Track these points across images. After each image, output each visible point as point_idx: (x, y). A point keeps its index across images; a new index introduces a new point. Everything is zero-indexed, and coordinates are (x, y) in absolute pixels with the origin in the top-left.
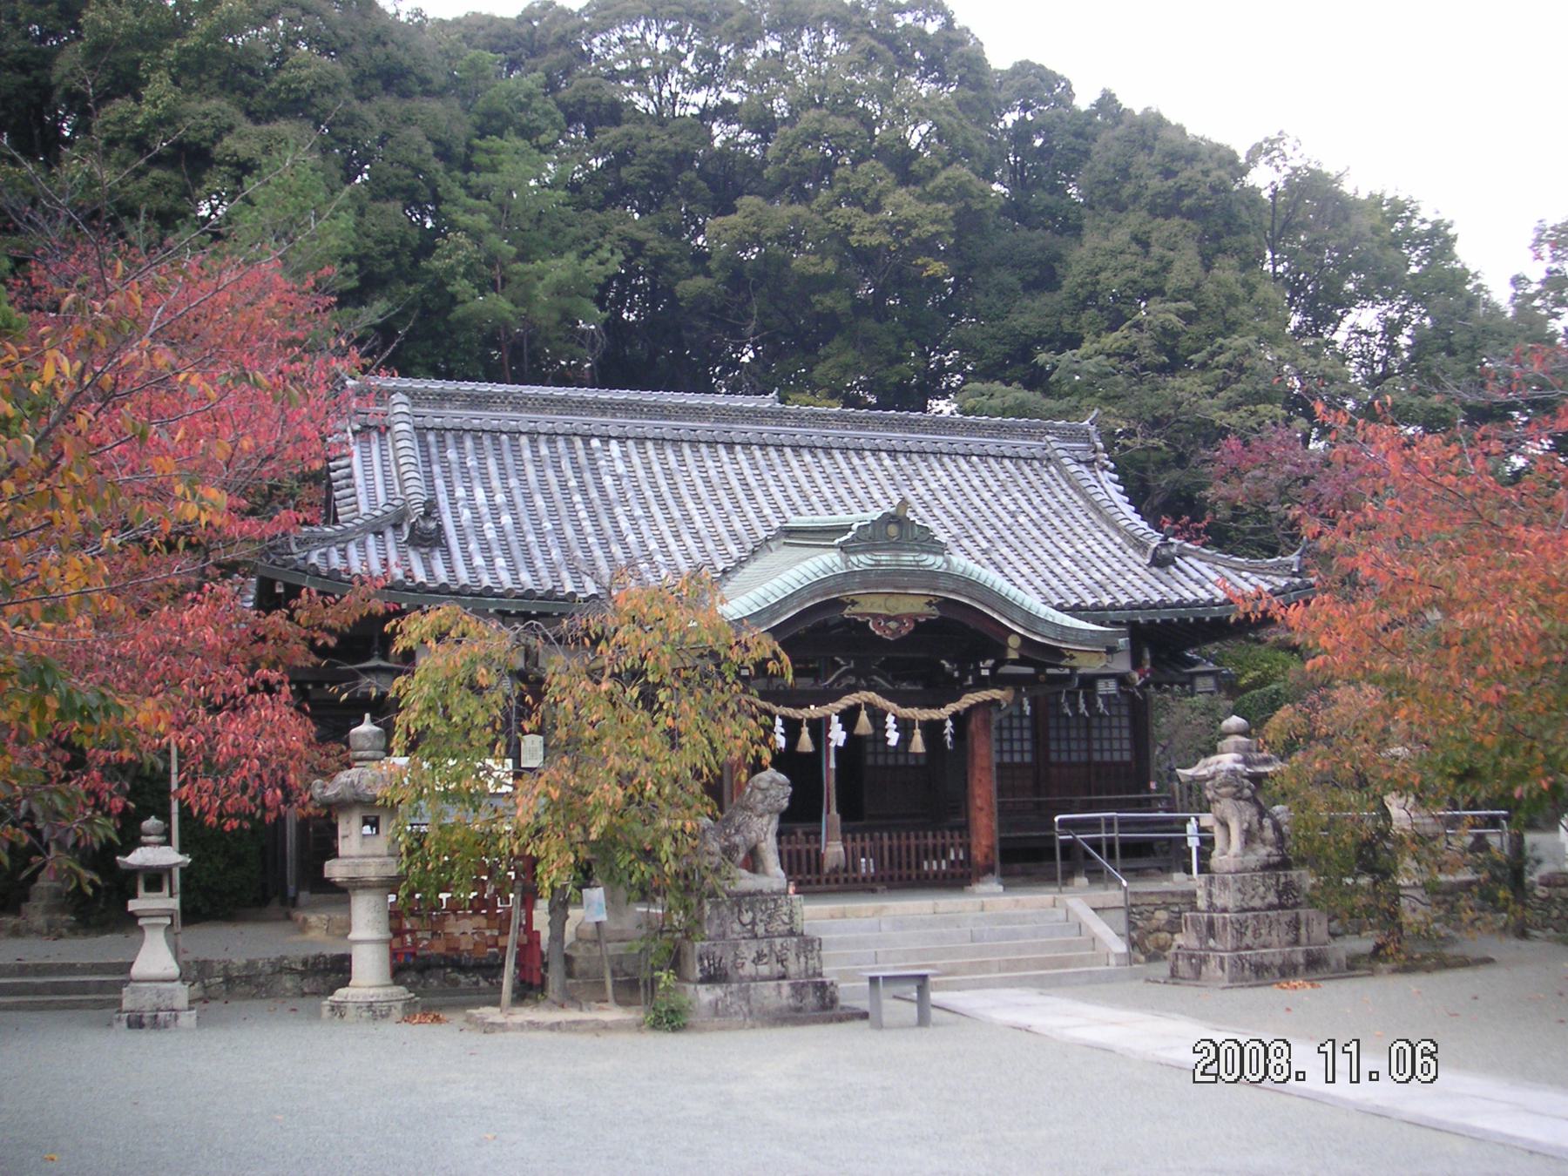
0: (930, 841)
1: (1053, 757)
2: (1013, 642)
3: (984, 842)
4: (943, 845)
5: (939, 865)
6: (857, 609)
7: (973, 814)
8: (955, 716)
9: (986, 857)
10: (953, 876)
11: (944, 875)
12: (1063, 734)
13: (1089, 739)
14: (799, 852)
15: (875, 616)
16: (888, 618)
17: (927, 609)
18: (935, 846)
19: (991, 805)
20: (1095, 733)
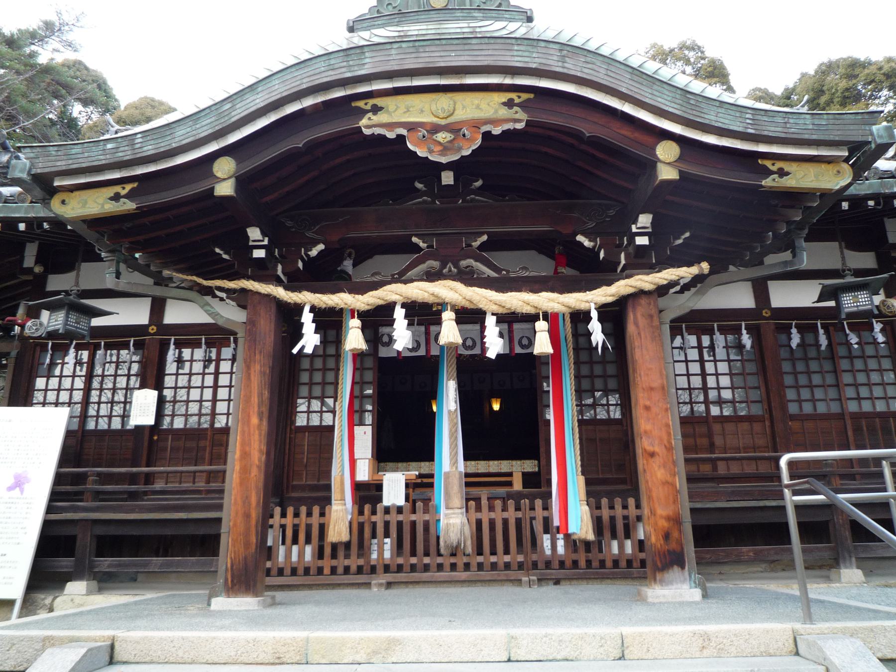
0: (619, 511)
1: (793, 408)
2: (666, 152)
3: (661, 511)
4: (626, 518)
5: (621, 547)
6: (382, 118)
7: (641, 463)
8: (605, 312)
9: (667, 536)
10: (643, 563)
11: (629, 563)
12: (803, 380)
13: (835, 371)
14: (413, 524)
15: (412, 127)
16: (435, 129)
17: (504, 112)
18: (612, 519)
19: (670, 449)
20: (847, 378)
